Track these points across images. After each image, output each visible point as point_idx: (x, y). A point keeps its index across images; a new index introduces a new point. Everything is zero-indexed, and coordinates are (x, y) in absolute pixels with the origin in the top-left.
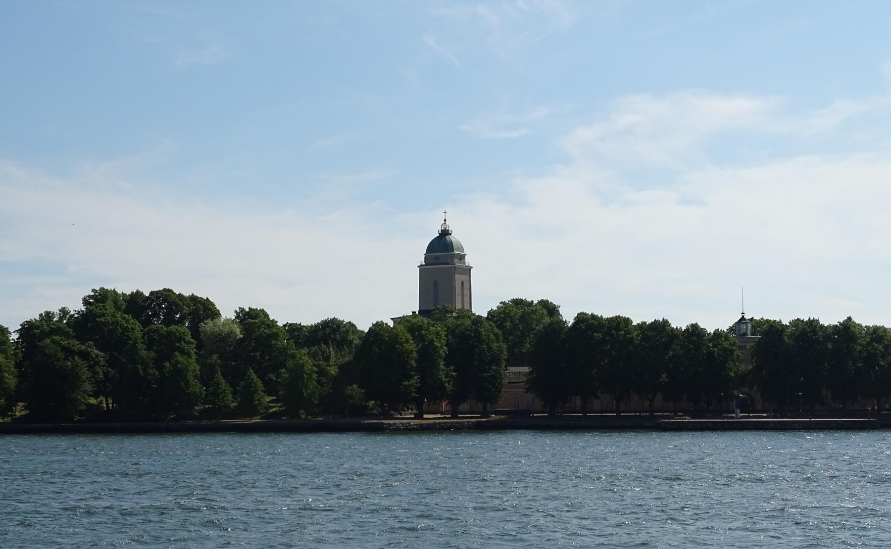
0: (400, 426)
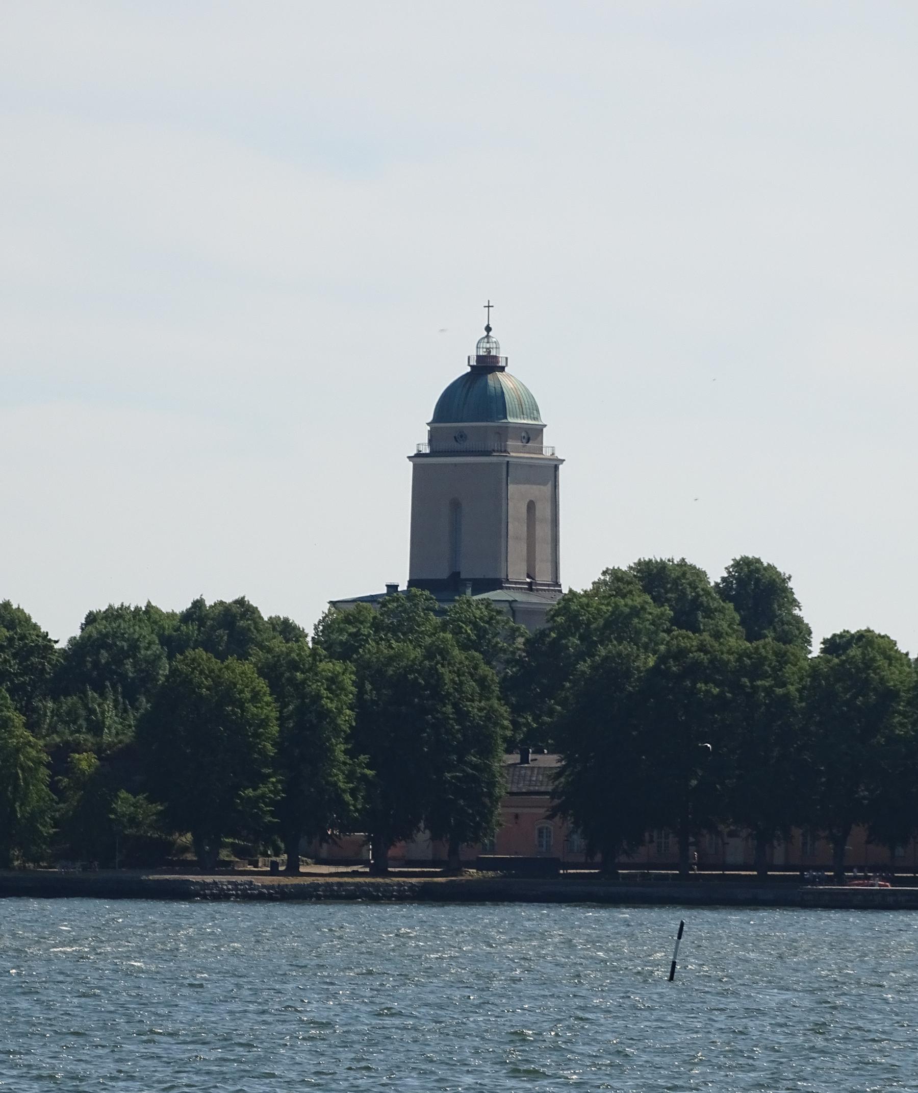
0: (229, 890)
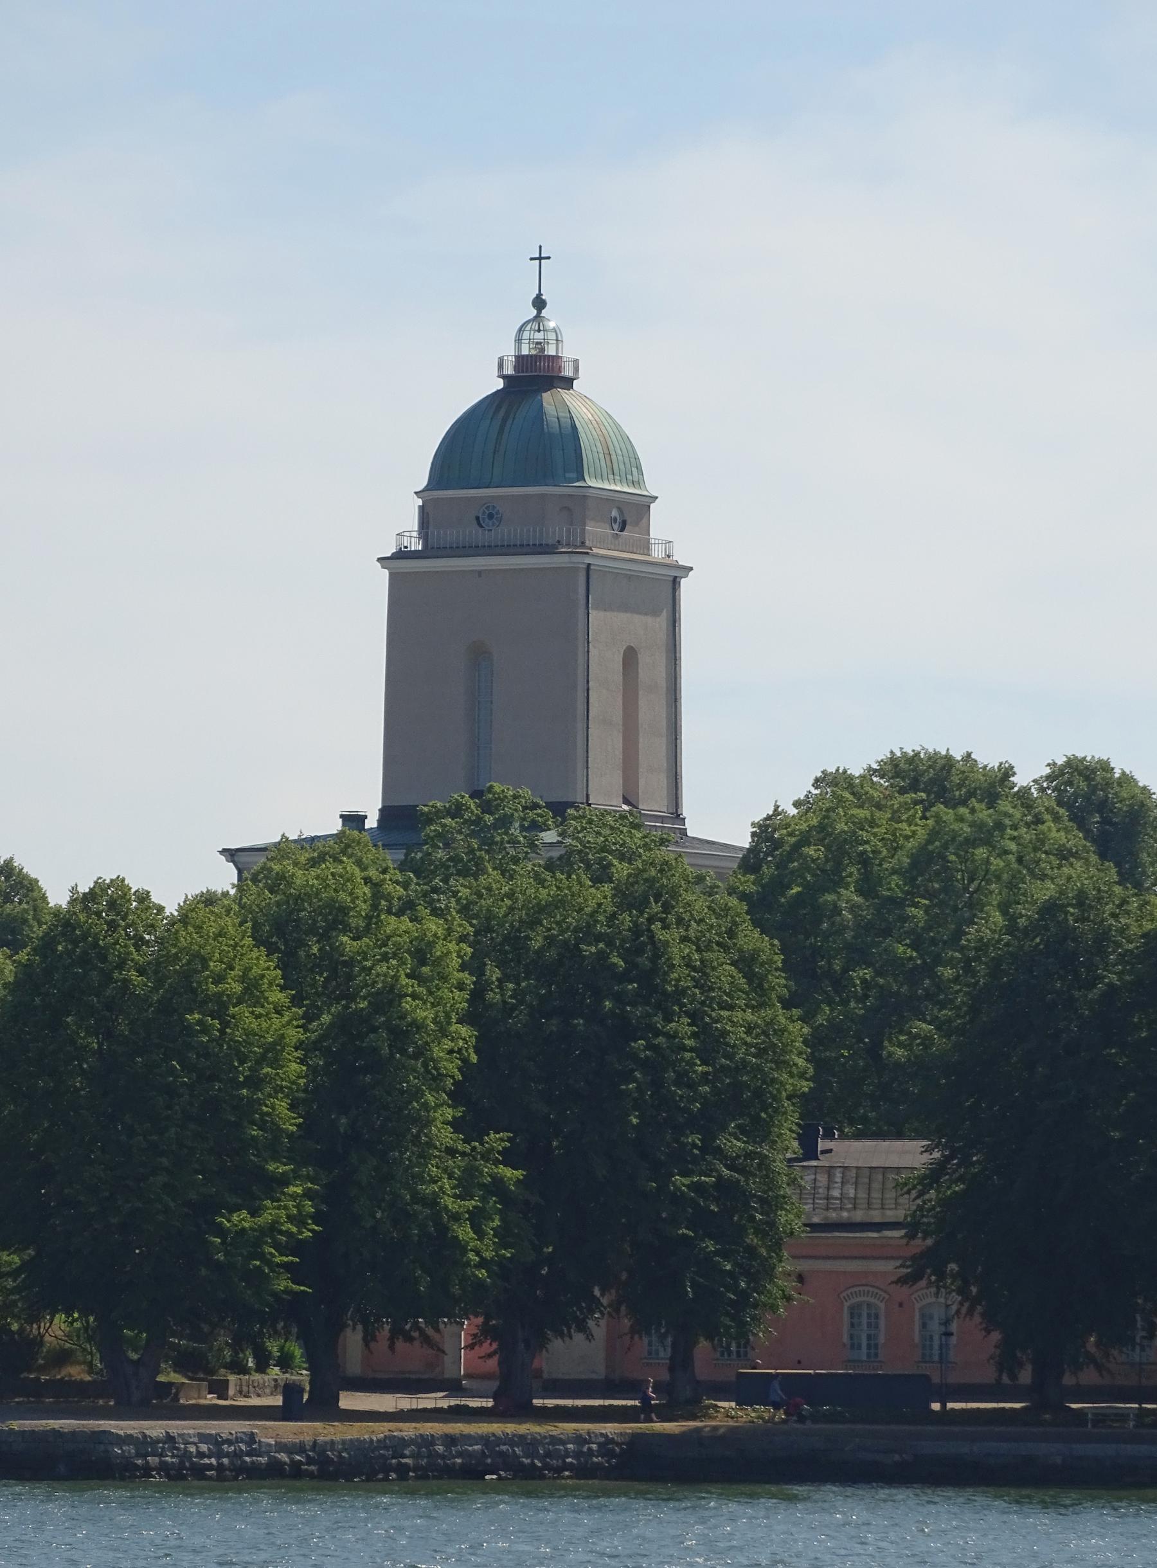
0: (201, 1455)
